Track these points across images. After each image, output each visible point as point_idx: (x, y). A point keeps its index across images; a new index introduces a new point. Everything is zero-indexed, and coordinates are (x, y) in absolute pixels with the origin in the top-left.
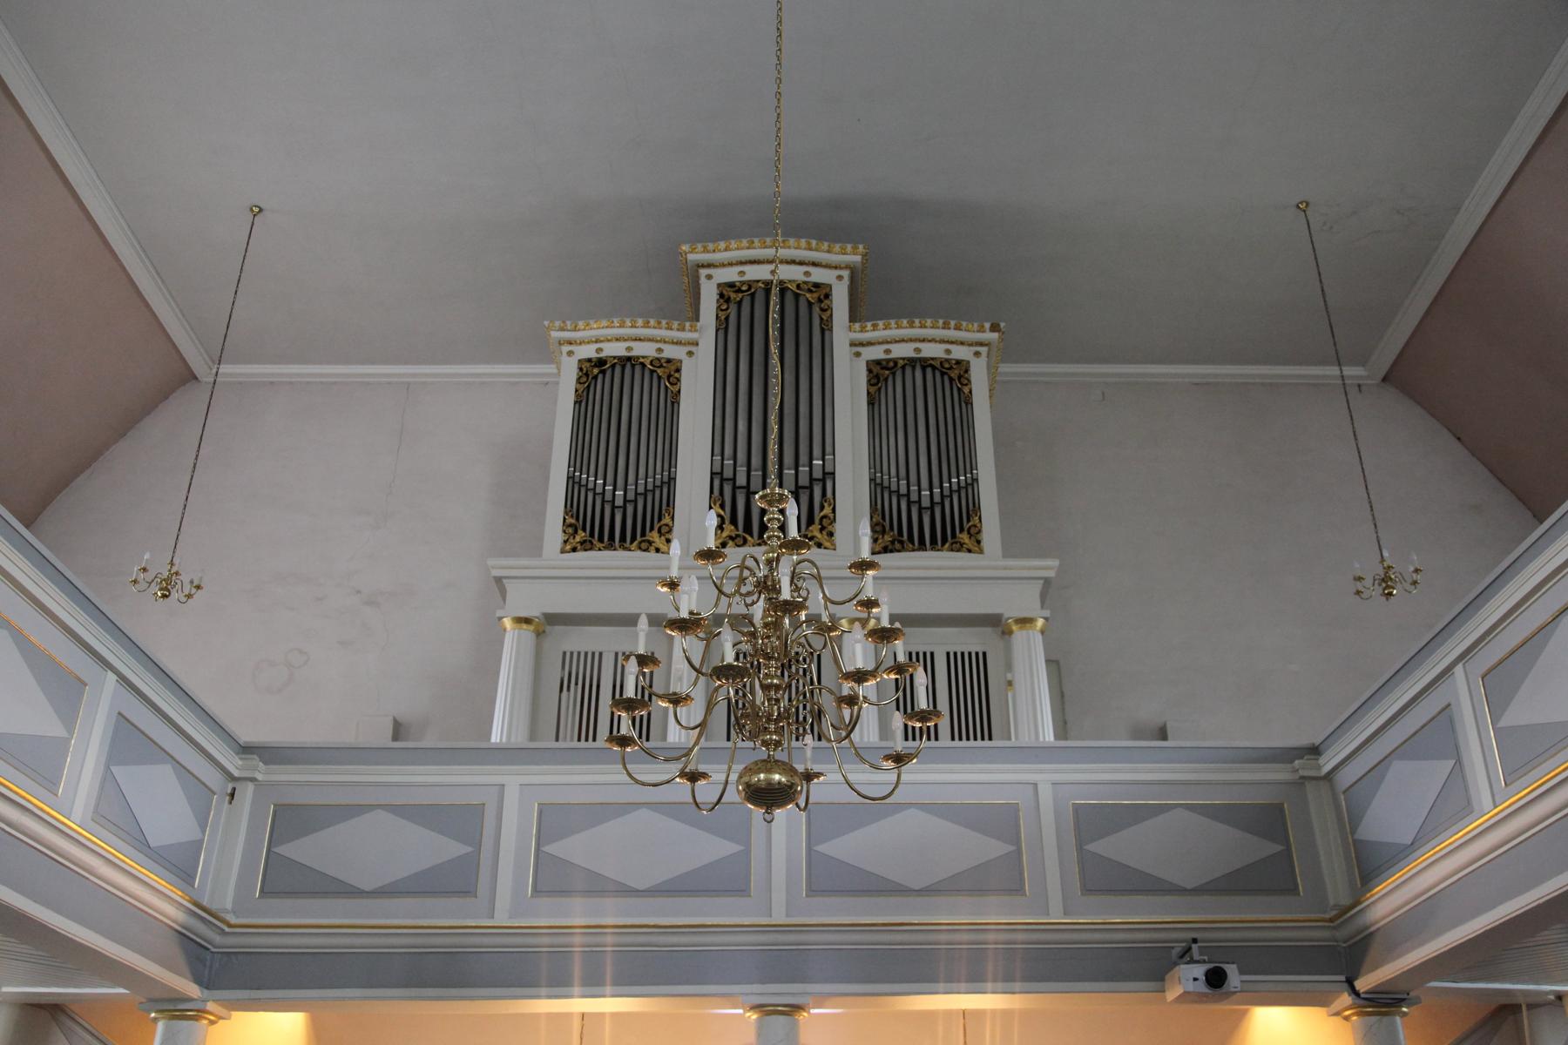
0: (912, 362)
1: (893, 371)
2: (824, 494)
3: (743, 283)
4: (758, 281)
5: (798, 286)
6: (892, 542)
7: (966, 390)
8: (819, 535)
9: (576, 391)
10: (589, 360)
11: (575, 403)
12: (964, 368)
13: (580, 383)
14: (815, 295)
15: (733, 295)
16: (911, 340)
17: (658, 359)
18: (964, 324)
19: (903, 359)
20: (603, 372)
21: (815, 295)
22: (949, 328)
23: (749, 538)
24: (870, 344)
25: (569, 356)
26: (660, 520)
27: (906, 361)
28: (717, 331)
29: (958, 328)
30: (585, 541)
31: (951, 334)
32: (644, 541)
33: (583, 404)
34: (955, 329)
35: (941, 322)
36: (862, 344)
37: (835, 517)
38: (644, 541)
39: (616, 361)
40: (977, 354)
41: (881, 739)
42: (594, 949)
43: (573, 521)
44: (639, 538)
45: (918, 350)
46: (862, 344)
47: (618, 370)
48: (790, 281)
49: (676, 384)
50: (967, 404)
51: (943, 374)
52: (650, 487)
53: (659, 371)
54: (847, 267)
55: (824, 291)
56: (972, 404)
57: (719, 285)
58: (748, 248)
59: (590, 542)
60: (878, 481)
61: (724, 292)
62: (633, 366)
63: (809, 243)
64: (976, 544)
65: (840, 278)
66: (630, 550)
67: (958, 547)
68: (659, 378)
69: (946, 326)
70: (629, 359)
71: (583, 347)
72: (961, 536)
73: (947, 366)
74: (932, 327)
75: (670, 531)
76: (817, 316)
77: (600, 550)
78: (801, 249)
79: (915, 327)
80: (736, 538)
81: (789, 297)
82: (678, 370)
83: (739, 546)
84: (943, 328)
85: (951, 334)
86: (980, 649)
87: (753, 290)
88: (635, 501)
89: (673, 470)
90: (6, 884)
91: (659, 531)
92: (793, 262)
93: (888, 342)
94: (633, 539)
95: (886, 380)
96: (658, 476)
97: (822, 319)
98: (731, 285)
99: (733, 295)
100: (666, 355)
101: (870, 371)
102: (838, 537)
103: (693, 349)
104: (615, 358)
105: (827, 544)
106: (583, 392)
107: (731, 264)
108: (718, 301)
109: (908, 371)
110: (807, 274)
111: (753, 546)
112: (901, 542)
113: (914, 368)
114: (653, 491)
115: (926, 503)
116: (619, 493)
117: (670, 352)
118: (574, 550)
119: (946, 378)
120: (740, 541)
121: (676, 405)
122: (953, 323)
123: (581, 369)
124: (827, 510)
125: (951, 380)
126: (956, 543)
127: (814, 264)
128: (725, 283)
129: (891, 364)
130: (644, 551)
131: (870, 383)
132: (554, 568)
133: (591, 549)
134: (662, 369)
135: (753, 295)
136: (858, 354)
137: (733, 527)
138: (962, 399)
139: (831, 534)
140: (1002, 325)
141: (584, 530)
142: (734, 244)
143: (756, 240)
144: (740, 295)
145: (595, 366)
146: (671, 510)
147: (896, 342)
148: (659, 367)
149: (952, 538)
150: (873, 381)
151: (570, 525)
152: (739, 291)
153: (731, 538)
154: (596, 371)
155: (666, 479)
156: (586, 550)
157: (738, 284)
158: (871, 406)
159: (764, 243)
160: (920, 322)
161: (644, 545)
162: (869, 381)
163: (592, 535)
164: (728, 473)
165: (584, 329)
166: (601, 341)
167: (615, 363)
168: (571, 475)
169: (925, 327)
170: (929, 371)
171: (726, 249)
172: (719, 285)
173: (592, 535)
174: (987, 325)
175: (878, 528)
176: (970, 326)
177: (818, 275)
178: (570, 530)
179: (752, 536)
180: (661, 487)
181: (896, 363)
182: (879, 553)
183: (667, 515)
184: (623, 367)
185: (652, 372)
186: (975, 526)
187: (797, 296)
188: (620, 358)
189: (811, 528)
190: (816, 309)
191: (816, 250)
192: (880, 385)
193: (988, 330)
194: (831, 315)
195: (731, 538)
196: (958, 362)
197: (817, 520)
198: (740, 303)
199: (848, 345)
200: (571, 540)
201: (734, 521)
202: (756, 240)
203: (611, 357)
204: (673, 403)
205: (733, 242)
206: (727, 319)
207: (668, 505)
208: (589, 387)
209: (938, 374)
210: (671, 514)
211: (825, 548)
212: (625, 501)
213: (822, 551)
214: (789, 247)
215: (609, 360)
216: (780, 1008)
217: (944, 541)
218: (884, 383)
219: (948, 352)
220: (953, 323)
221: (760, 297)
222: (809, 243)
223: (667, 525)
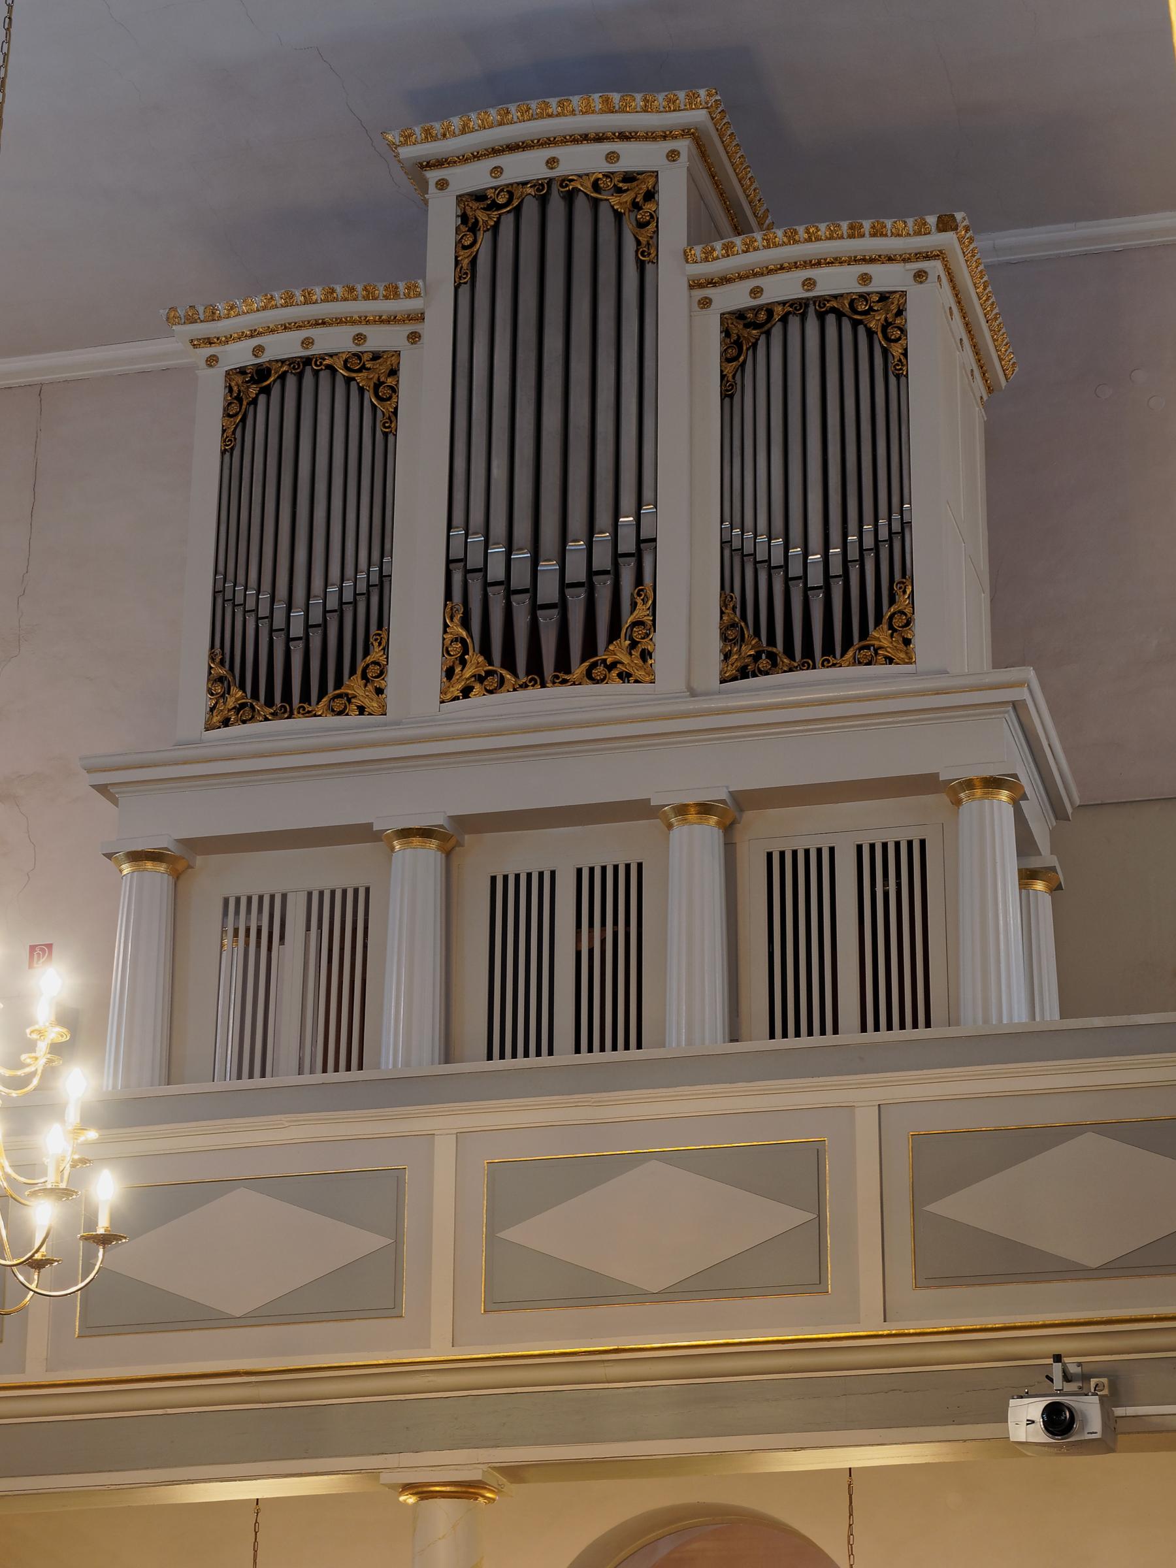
0: (799, 307)
1: (766, 328)
2: (639, 580)
3: (499, 190)
4: (524, 184)
5: (596, 186)
6: (756, 658)
7: (896, 350)
8: (625, 659)
9: (224, 431)
10: (242, 371)
11: (223, 453)
12: (894, 308)
13: (229, 416)
14: (627, 198)
15: (482, 216)
16: (795, 266)
17: (358, 356)
18: (889, 223)
19: (784, 303)
20: (267, 391)
21: (627, 198)
23: (508, 676)
24: (725, 280)
25: (210, 366)
26: (366, 653)
27: (788, 309)
28: (456, 289)
29: (877, 233)
30: (243, 706)
31: (868, 245)
32: (340, 696)
33: (237, 452)
34: (873, 235)
35: (845, 225)
36: (712, 283)
37: (654, 621)
38: (340, 696)
39: (285, 368)
40: (920, 276)
41: (1063, 1015)
42: (169, 1411)
43: (222, 672)
44: (331, 692)
45: (809, 283)
46: (712, 283)
47: (291, 381)
48: (580, 176)
49: (390, 398)
50: (898, 377)
51: (855, 324)
52: (348, 596)
53: (359, 377)
54: (686, 132)
56: (907, 376)
57: (460, 198)
58: (501, 124)
59: (253, 708)
60: (736, 544)
61: (469, 213)
62: (316, 373)
63: (607, 101)
64: (902, 646)
65: (673, 155)
66: (315, 716)
67: (871, 656)
68: (361, 390)
69: (855, 232)
70: (307, 361)
71: (232, 347)
72: (876, 634)
73: (862, 307)
74: (831, 238)
75: (382, 673)
77: (266, 719)
78: (593, 112)
80: (485, 678)
81: (581, 204)
82: (393, 372)
83: (491, 692)
84: (851, 236)
85: (868, 245)
86: (361, 883)
87: (515, 203)
88: (324, 625)
89: (647, 509)
91: (364, 676)
92: (585, 138)
93: (755, 275)
94: (323, 692)
95: (754, 346)
96: (362, 576)
97: (639, 243)
98: (479, 197)
99: (482, 216)
100: (372, 345)
101: (726, 333)
102: (659, 660)
104: (283, 362)
105: (639, 674)
106: (234, 433)
107: (476, 157)
108: (457, 229)
109: (794, 323)
110: (612, 157)
111: (515, 690)
112: (772, 657)
113: (803, 318)
114: (355, 603)
115: (815, 578)
116: (548, 566)
117: (379, 339)
118: (226, 723)
119: (861, 330)
120: (492, 682)
121: (391, 437)
122: (867, 225)
123: (231, 390)
124: (642, 612)
125: (870, 334)
126: (868, 647)
127: (624, 136)
128: (470, 194)
129: (762, 316)
130: (340, 713)
131: (726, 359)
132: (185, 763)
133: (252, 719)
134: (364, 374)
135: (518, 210)
136: (705, 303)
137: (481, 659)
138: (891, 369)
139: (646, 655)
140: (959, 216)
141: (242, 687)
142: (474, 119)
143: (513, 108)
144: (495, 214)
145: (253, 381)
146: (384, 635)
147: (770, 272)
148: (359, 371)
149: (860, 640)
150: (733, 352)
151: (221, 679)
152: (494, 206)
153: (480, 679)
154: (253, 391)
155: (375, 579)
156: (244, 722)
157: (490, 193)
158: (727, 400)
159: (528, 109)
160: (807, 231)
161: (338, 705)
162: (724, 352)
163: (255, 695)
164: (475, 560)
165: (228, 317)
166: (260, 334)
167: (285, 373)
168: (219, 587)
169: (818, 239)
170: (831, 319)
171: (464, 130)
172: (460, 198)
173: (255, 695)
174: (932, 220)
175: (731, 634)
176: (901, 225)
177: (633, 157)
178: (219, 689)
179: (514, 673)
180: (368, 595)
181: (770, 313)
182: (734, 679)
183: (376, 644)
184: (300, 377)
185: (348, 380)
186: (902, 613)
187: (595, 203)
188: (291, 362)
189: (611, 647)
191: (622, 111)
192: (742, 358)
193: (934, 229)
194: (656, 232)
195: (480, 679)
196: (884, 297)
197: (359, 671)
198: (495, 229)
199: (686, 285)
200: (221, 707)
201: (486, 651)
202: (513, 108)
203: (277, 361)
204: (386, 435)
205: (473, 116)
206: (473, 262)
207: (380, 626)
208: (243, 420)
209: (847, 326)
211: (636, 681)
212: (307, 627)
213: (630, 687)
214: (573, 113)
215: (274, 366)
216: (437, 1489)
217: (847, 643)
218: (750, 352)
219: (865, 279)
220: (867, 225)
221: (531, 210)
222: (607, 101)
223: (376, 663)
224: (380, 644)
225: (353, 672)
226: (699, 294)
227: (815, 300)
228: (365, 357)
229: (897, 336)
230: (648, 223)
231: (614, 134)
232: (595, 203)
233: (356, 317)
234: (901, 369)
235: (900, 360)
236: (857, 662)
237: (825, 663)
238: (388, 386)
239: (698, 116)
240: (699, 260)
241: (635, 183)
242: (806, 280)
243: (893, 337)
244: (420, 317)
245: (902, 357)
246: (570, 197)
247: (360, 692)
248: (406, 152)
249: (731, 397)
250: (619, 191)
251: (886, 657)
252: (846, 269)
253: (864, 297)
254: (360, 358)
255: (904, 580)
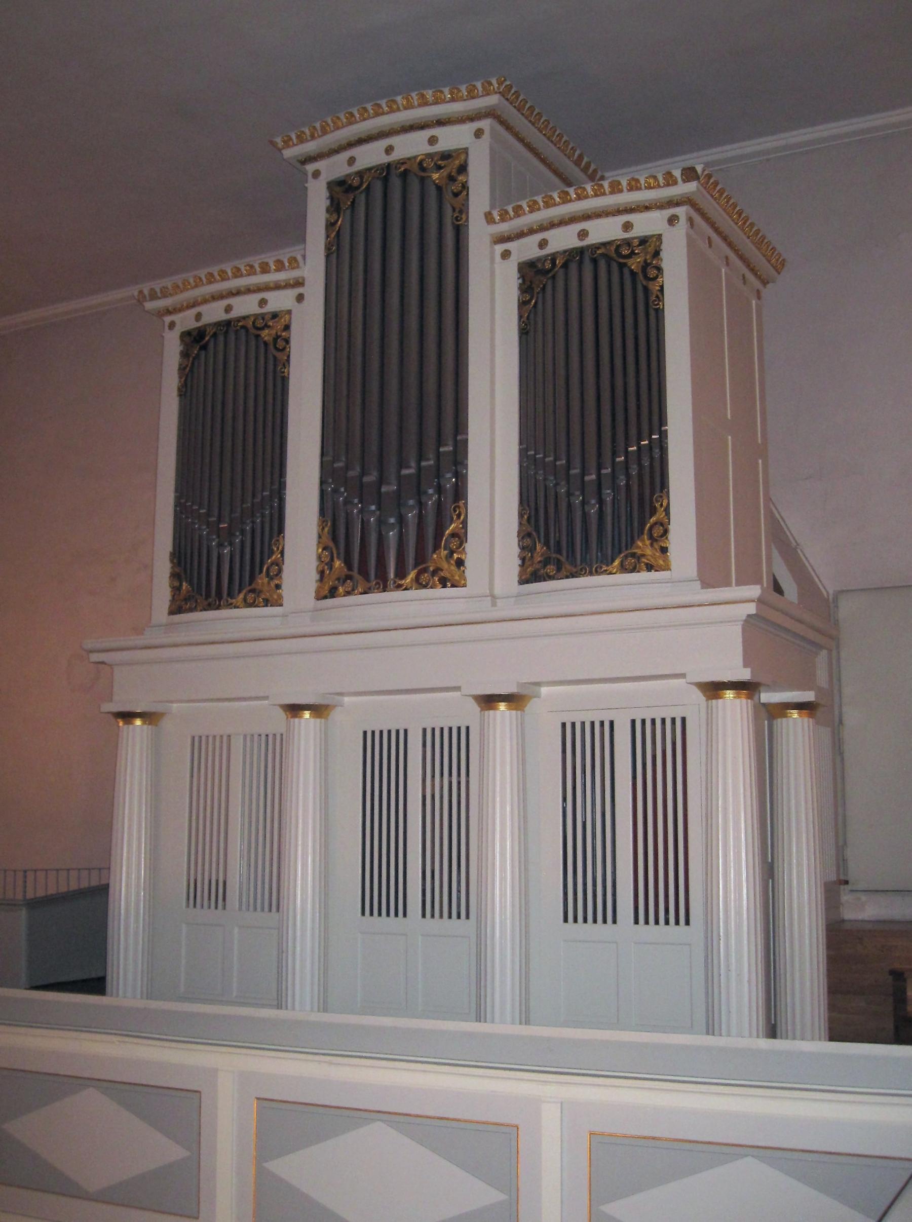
12: (651, 250)
14: (444, 173)
20: (204, 348)
22: (621, 191)
47: (573, 267)
55: (457, 162)
62: (236, 332)
73: (625, 252)
76: (449, 206)
79: (571, 201)
82: (287, 328)
90: (0, 986)
103: (300, 290)
119: (626, 271)
127: (440, 123)
129: (548, 265)
144: (351, 196)
169: (587, 197)
173: (559, 551)
190: (448, 196)
191: (436, 103)
193: (679, 180)
196: (643, 241)
209: (615, 268)
210: (280, 548)
218: (540, 295)
221: (378, 187)
224: (278, 549)
225: (261, 571)
226: (499, 248)
227: (588, 247)
228: (266, 317)
229: (655, 275)
230: (461, 192)
231: (433, 122)
232: (422, 180)
233: (272, 285)
234: (658, 304)
235: (657, 297)
236: (623, 569)
237: (598, 570)
238: (283, 339)
239: (493, 100)
240: (662, 185)
241: (450, 160)
242: (580, 232)
243: (651, 277)
244: (299, 283)
245: (659, 293)
246: (405, 175)
247: (649, 551)
248: (288, 153)
249: (527, 333)
250: (439, 168)
251: (647, 564)
252: (610, 220)
253: (628, 243)
254: (263, 319)
255: (661, 494)
